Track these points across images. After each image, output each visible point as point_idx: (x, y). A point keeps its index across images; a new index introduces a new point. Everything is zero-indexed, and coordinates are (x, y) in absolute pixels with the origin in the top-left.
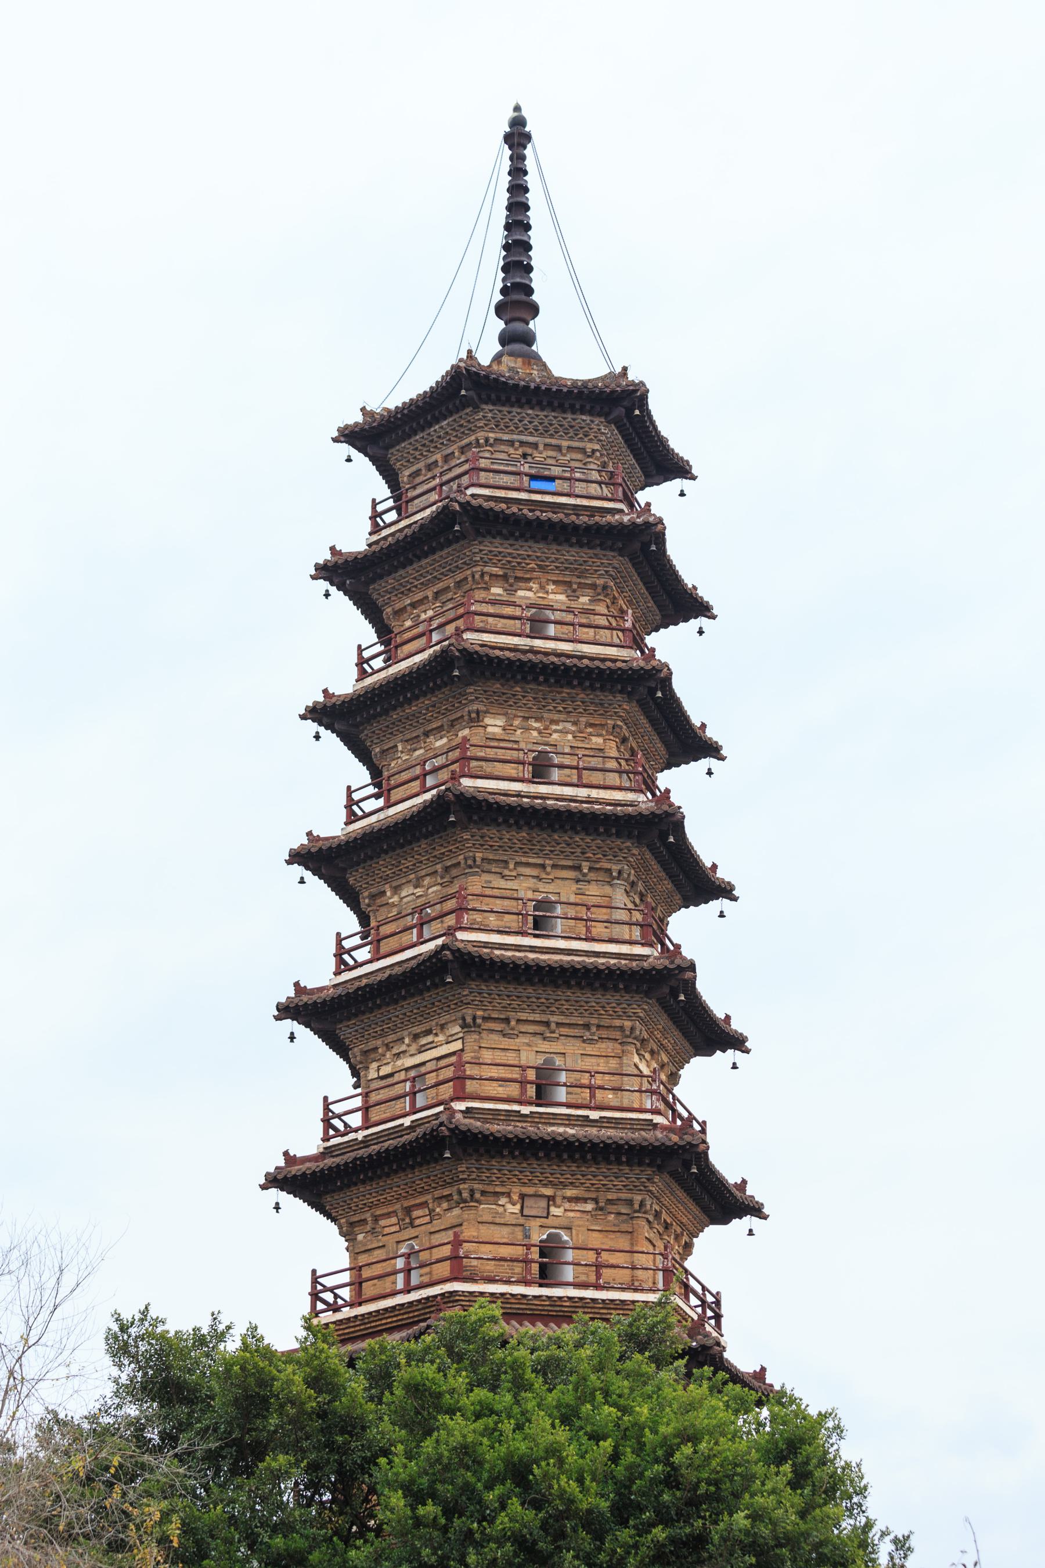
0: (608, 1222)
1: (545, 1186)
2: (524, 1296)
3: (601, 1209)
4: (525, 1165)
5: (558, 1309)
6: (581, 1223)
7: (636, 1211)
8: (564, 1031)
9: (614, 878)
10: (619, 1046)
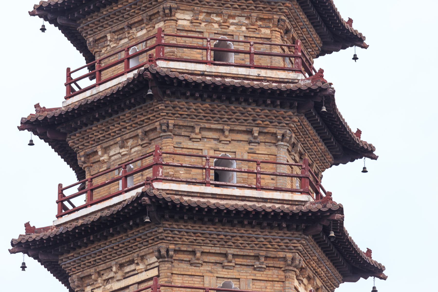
9: (278, 140)
10: (282, 273)
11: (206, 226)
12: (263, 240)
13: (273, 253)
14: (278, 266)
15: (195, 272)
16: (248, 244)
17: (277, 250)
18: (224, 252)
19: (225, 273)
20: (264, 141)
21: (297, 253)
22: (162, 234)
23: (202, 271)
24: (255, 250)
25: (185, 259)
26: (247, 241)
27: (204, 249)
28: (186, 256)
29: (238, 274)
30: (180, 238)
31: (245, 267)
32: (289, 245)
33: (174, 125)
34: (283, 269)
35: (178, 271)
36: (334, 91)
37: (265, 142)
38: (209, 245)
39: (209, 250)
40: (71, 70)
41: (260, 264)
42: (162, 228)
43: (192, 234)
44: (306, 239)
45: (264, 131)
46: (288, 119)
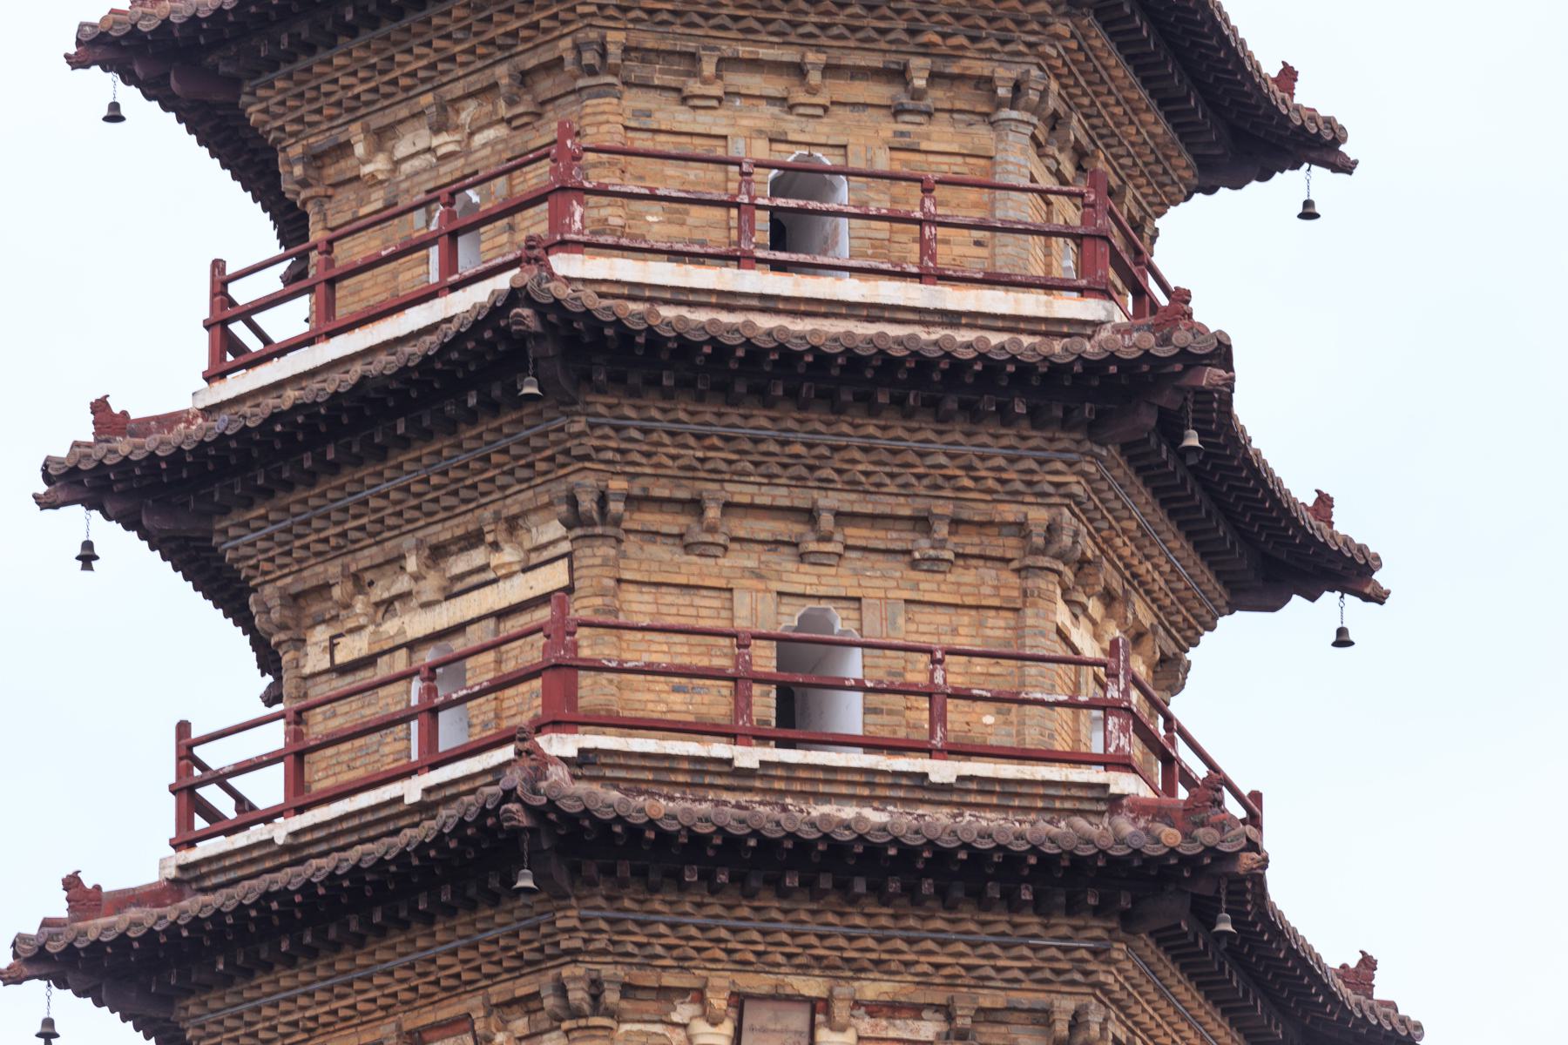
1: (803, 969)
4: (746, 912)
8: (858, 534)
9: (1000, 104)
10: (1014, 580)
11: (742, 411)
12: (943, 460)
14: (998, 553)
15: (701, 575)
16: (892, 476)
17: (995, 496)
18: (806, 504)
19: (807, 579)
20: (947, 106)
22: (584, 440)
23: (726, 572)
24: (917, 495)
25: (665, 529)
27: (733, 493)
28: (669, 518)
30: (648, 455)
32: (1036, 478)
33: (627, 50)
35: (639, 570)
36: (1266, 860)
37: (951, 111)
39: (753, 495)
40: (229, 271)
41: (933, 547)
42: (583, 419)
43: (692, 441)
44: (1098, 457)
45: (948, 70)
46: (1035, 26)
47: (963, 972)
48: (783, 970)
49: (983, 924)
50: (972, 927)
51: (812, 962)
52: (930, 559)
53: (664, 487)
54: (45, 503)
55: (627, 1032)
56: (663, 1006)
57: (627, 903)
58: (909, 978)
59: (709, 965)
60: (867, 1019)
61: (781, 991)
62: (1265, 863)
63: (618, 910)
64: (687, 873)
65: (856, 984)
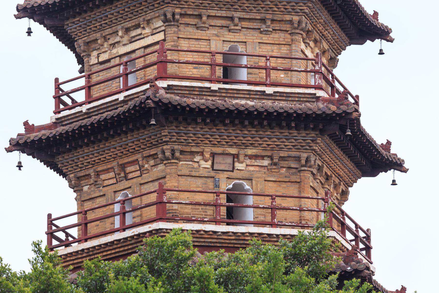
0: (281, 174)
1: (231, 146)
2: (215, 232)
3: (275, 164)
4: (215, 130)
5: (242, 242)
6: (260, 175)
7: (303, 166)
8: (245, 24)
10: (289, 36)
13: (280, 16)
14: (284, 29)
15: (201, 36)
16: (255, 7)
17: (284, 13)
18: (230, 16)
19: (231, 37)
21: (304, 16)
23: (208, 35)
25: (191, 23)
26: (253, 4)
27: (210, 13)
28: (192, 20)
29: (244, 37)
31: (252, 30)
32: (295, 8)
34: (289, 32)
36: (360, 114)
38: (215, 9)
39: (216, 13)
41: (266, 28)
47: (275, 147)
48: (225, 146)
49: (281, 133)
50: (278, 134)
51: (233, 144)
52: (265, 31)
53: (191, 11)
54: (17, 17)
55: (182, 164)
56: (192, 157)
57: (181, 128)
58: (261, 148)
59: (205, 145)
60: (249, 160)
61: (225, 152)
62: (360, 115)
63: (179, 130)
64: (198, 119)
65: (246, 150)
